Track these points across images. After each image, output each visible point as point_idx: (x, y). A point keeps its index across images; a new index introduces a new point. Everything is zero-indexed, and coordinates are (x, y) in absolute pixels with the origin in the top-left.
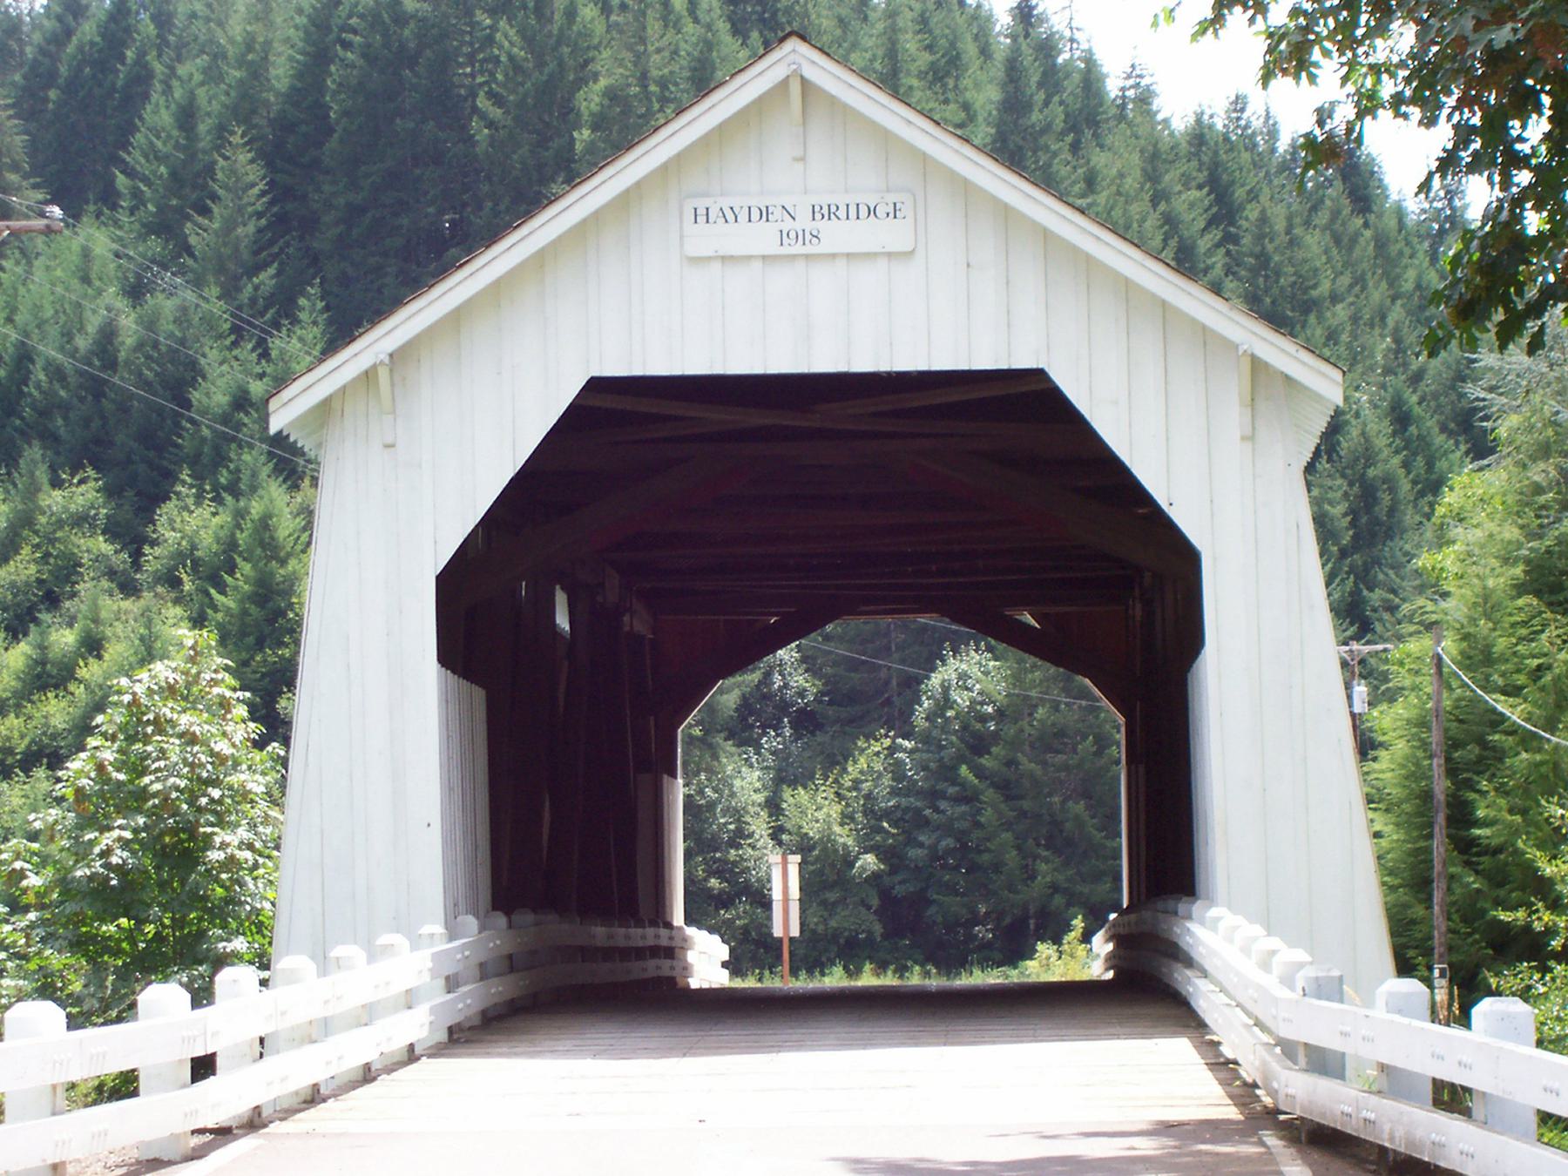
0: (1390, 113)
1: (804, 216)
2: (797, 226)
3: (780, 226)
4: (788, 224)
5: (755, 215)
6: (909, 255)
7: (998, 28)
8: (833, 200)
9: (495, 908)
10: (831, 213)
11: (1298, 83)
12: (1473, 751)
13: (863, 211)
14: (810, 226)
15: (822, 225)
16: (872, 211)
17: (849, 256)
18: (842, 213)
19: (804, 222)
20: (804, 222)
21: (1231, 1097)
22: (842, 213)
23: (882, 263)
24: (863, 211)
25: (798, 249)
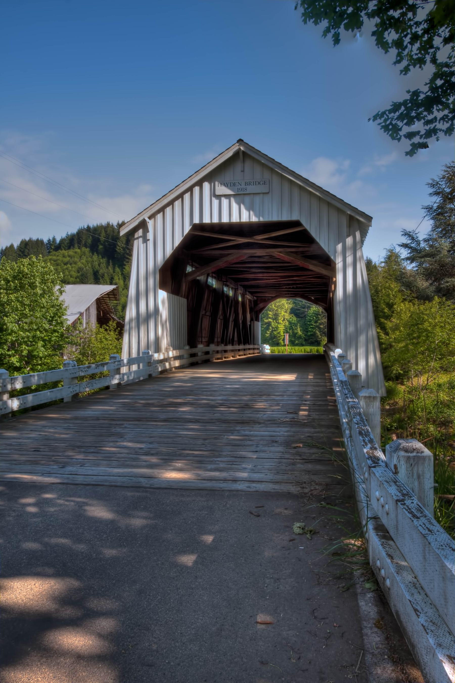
0: (419, 137)
1: (243, 184)
2: (242, 187)
3: (238, 187)
4: (239, 187)
5: (232, 184)
6: (268, 193)
7: (369, 595)
8: (250, 181)
9: (30, 239)
10: (250, 184)
11: (395, 63)
12: (443, 325)
13: (257, 183)
14: (244, 187)
15: (247, 187)
16: (259, 183)
17: (254, 194)
18: (252, 184)
19: (243, 186)
20: (243, 186)
21: (67, 250)
22: (252, 184)
23: (261, 195)
24: (257, 183)
25: (242, 192)
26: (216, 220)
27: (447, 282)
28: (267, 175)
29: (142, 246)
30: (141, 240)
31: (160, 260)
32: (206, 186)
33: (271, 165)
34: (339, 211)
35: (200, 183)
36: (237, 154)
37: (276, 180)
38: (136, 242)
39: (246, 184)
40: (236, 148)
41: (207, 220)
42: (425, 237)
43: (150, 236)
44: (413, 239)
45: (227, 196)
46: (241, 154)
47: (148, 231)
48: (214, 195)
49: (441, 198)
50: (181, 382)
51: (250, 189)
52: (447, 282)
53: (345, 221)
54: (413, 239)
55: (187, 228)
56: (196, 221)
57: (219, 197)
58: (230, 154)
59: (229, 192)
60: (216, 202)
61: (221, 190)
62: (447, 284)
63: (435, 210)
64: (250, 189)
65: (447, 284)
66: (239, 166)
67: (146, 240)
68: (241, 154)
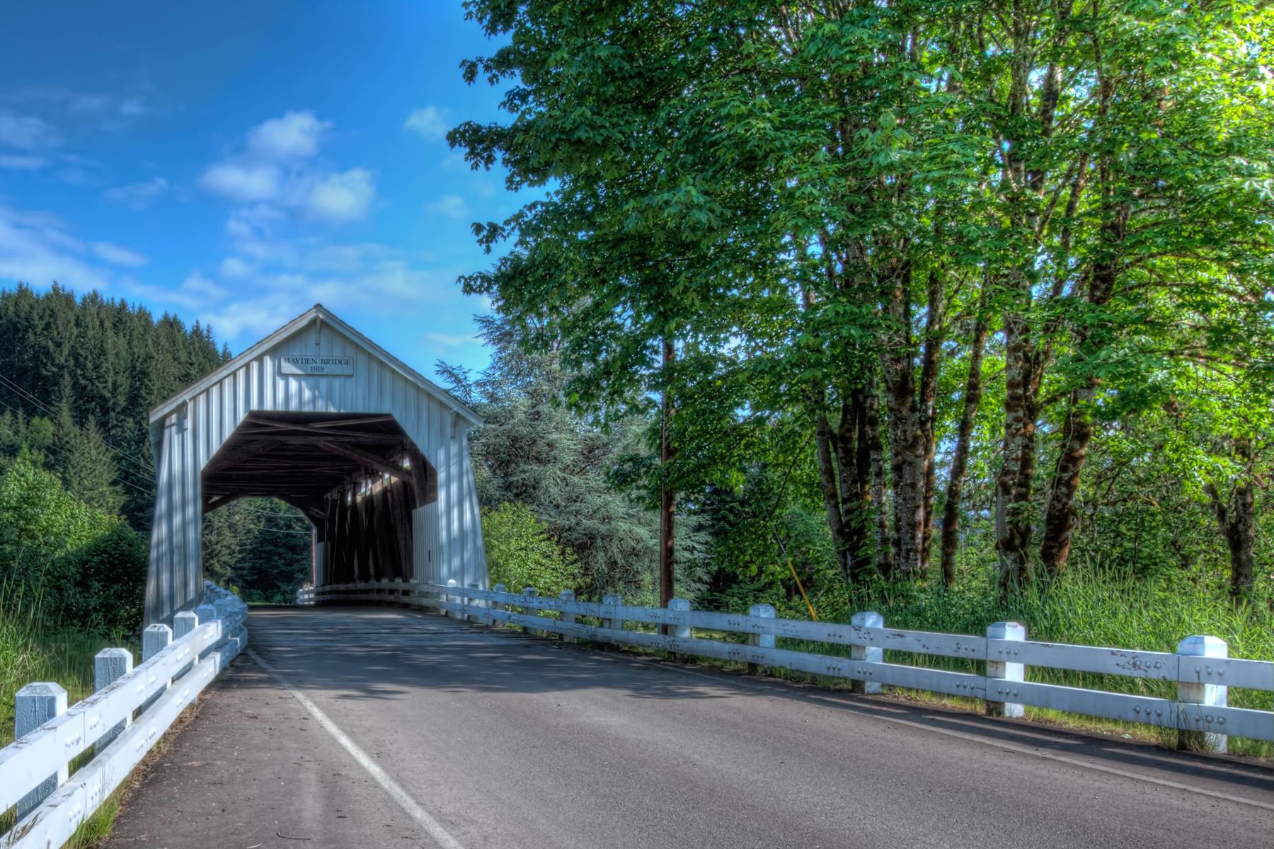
10: (327, 362)
19: (319, 364)
26: (281, 408)
27: (525, 472)
28: (350, 352)
29: (176, 440)
30: (174, 429)
31: (203, 463)
32: (268, 362)
33: (357, 341)
34: (442, 405)
35: (260, 359)
36: (313, 323)
37: (362, 359)
38: (167, 432)
39: (322, 361)
40: (312, 315)
41: (268, 406)
42: (479, 377)
43: (189, 424)
44: (458, 381)
45: (294, 375)
46: (318, 323)
47: (186, 417)
48: (278, 372)
49: (705, 519)
50: (1060, 761)
51: (329, 369)
52: (525, 472)
53: (449, 420)
54: (458, 381)
55: (242, 416)
56: (254, 406)
57: (285, 376)
58: (305, 322)
59: (298, 372)
60: (281, 384)
61: (288, 368)
62: (524, 476)
63: (498, 328)
64: (329, 369)
65: (524, 476)
66: (312, 337)
67: (181, 429)
68: (318, 323)
